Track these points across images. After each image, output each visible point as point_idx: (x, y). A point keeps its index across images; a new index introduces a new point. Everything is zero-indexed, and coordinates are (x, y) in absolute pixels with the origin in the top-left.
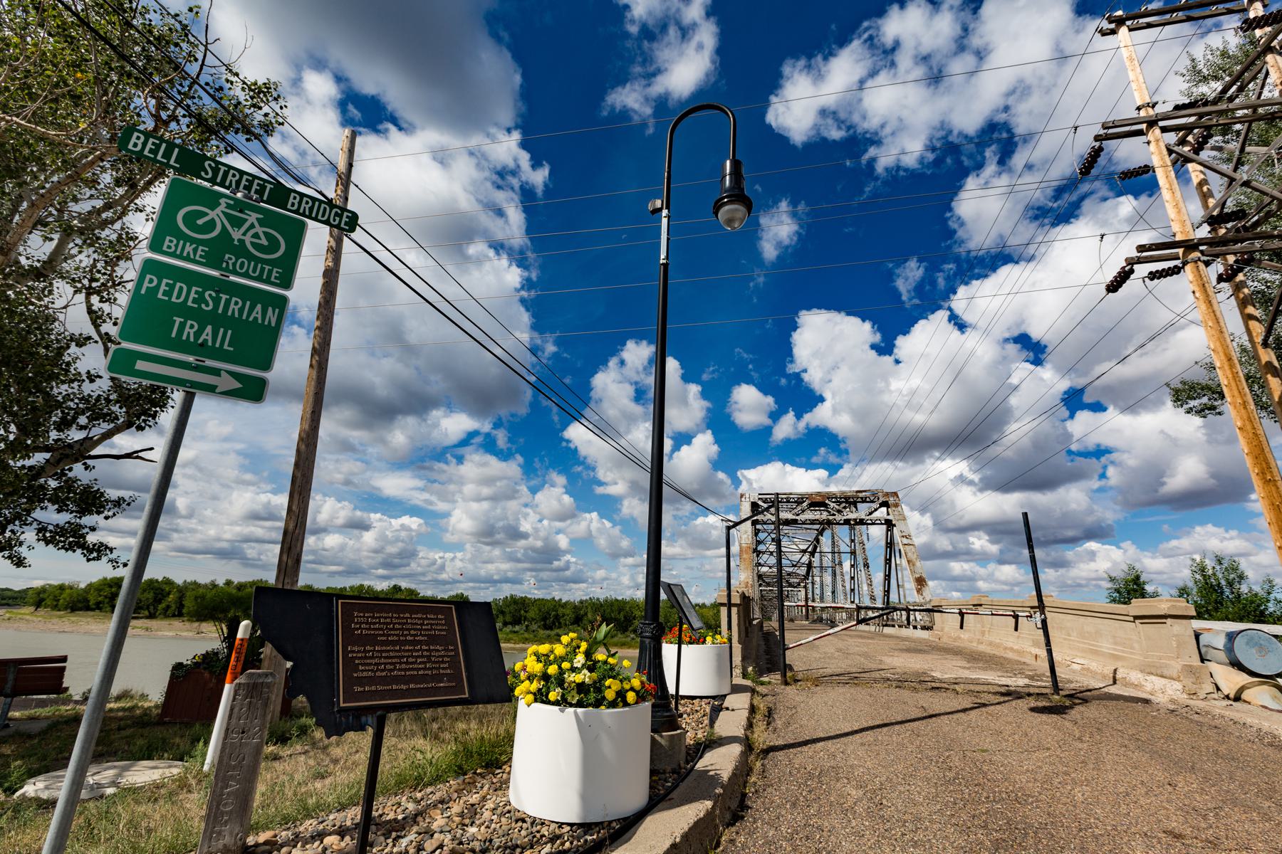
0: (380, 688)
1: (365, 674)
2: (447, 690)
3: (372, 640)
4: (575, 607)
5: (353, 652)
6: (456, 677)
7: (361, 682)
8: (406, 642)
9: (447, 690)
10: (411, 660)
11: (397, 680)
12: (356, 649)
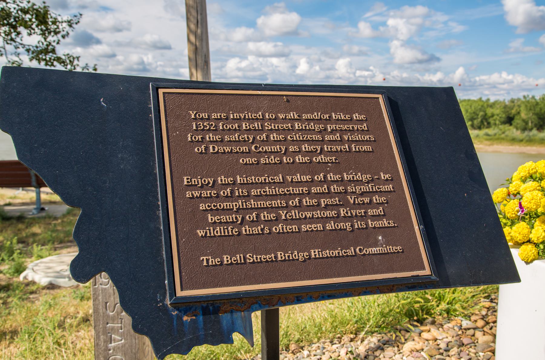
0: (251, 258)
1: (219, 231)
2: (387, 261)
3: (227, 163)
4: (505, 107)
5: (191, 186)
6: (398, 232)
7: (219, 245)
8: (293, 168)
9: (387, 261)
10: (306, 201)
11: (284, 241)
12: (359, 177)
